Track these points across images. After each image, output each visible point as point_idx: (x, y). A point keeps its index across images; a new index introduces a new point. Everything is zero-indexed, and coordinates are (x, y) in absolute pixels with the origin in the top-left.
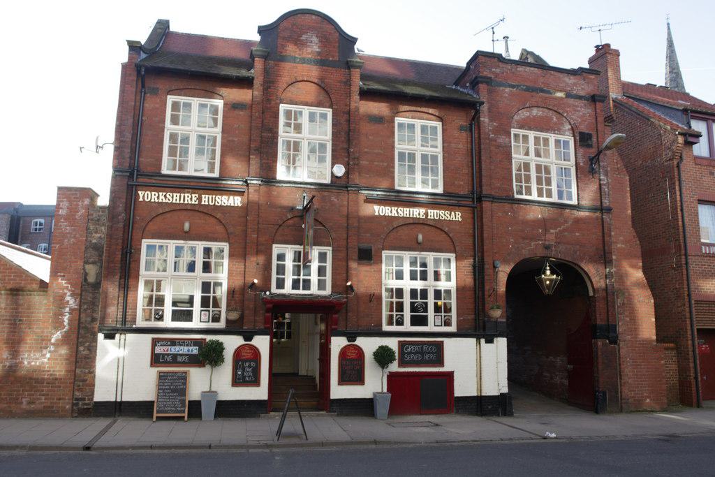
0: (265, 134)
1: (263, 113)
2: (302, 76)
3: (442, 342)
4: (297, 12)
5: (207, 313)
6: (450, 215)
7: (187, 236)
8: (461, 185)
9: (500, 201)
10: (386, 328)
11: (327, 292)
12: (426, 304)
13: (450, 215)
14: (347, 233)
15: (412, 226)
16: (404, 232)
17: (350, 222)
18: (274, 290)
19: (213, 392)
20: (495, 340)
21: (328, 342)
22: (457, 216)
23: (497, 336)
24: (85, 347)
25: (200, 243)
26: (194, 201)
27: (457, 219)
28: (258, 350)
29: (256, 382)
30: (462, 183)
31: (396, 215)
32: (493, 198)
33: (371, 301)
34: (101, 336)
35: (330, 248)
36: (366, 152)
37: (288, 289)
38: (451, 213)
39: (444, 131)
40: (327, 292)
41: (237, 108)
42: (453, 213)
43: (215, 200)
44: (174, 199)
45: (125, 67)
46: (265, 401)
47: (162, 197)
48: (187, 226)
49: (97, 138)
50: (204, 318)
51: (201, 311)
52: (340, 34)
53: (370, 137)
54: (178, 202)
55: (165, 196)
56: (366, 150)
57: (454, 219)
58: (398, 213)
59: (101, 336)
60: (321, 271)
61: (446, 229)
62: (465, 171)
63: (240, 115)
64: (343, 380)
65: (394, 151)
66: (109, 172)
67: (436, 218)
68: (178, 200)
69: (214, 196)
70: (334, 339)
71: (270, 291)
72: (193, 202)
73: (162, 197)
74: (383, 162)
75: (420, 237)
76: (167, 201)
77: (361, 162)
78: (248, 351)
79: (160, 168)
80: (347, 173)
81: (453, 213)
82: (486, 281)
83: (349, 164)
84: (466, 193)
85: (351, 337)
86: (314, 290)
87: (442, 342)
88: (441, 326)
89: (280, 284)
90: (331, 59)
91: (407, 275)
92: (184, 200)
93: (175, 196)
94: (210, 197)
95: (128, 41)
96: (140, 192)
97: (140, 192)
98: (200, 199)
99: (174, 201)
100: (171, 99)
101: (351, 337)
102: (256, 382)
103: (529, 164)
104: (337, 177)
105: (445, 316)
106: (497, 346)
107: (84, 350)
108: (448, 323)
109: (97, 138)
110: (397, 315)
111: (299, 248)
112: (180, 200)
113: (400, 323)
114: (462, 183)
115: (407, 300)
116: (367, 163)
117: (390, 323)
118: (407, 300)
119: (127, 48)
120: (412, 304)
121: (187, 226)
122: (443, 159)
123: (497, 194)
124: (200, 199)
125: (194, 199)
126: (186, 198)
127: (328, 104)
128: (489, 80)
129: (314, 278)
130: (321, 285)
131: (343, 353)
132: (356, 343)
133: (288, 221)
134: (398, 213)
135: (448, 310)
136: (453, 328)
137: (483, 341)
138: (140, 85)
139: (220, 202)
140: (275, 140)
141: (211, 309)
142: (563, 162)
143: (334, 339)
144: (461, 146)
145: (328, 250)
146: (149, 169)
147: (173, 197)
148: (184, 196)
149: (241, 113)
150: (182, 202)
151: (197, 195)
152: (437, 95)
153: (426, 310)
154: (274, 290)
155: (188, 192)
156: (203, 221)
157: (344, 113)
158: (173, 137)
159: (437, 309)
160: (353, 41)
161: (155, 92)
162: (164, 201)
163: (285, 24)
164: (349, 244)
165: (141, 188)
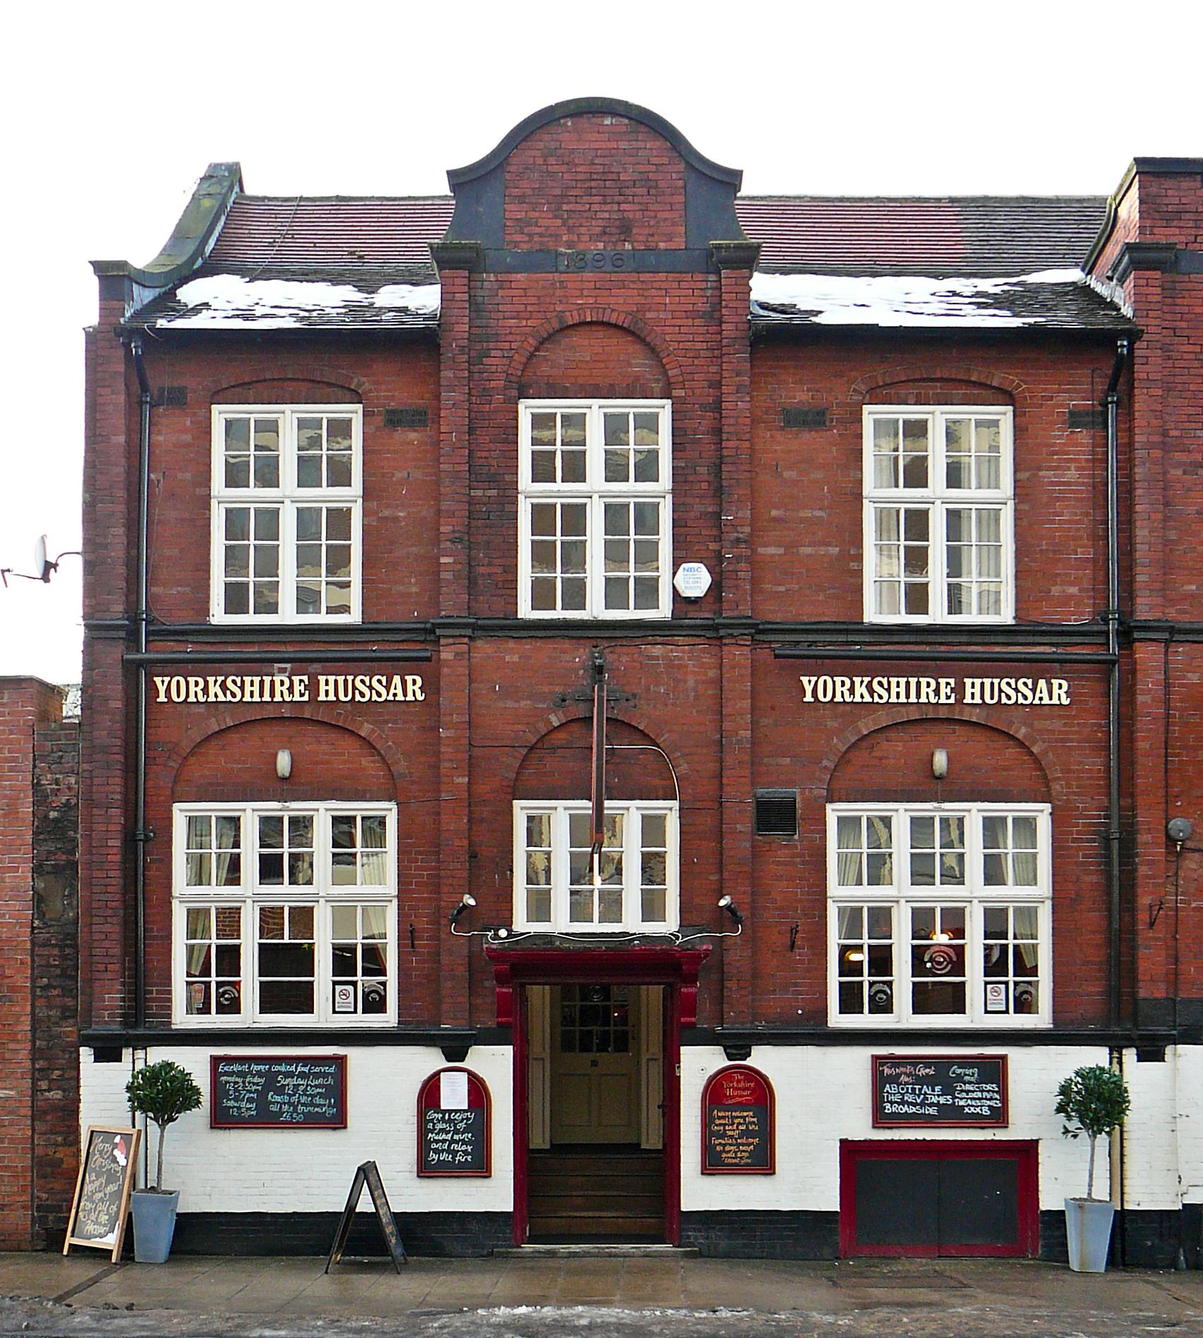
0: (480, 493)
1: (471, 431)
2: (581, 308)
3: (1004, 1058)
4: (621, 110)
5: (351, 988)
6: (1034, 690)
7: (288, 788)
8: (1072, 596)
9: (1190, 637)
10: (837, 1020)
11: (670, 924)
12: (960, 950)
13: (1034, 690)
14: (721, 761)
15: (919, 729)
16: (895, 749)
17: (726, 726)
18: (522, 923)
19: (165, 1192)
20: (1169, 1050)
21: (672, 1061)
22: (1058, 692)
23: (1175, 1042)
24: (51, 1081)
25: (901, 806)
26: (946, 696)
27: (1055, 701)
28: (764, 1078)
29: (480, 1167)
30: (1073, 590)
31: (868, 699)
32: (1172, 630)
33: (792, 947)
34: (86, 1054)
35: (675, 804)
36: (775, 519)
37: (561, 922)
38: (1035, 684)
39: (1019, 431)
40: (670, 924)
41: (399, 422)
42: (1042, 683)
43: (354, 688)
44: (247, 694)
45: (92, 338)
46: (510, 1212)
47: (860, 690)
48: (284, 762)
49: (43, 539)
50: (346, 1003)
51: (986, 983)
52: (690, 166)
53: (786, 474)
54: (257, 698)
55: (224, 687)
56: (774, 513)
57: (1046, 701)
58: (871, 692)
59: (86, 1054)
60: (652, 867)
61: (1021, 733)
62: (1084, 552)
63: (411, 443)
64: (713, 1164)
65: (515, 503)
66: (76, 635)
67: (988, 700)
68: (257, 694)
69: (350, 678)
70: (689, 1054)
71: (508, 924)
72: (297, 698)
73: (860, 690)
74: (829, 544)
75: (940, 760)
76: (229, 698)
77: (762, 550)
78: (742, 1085)
79: (206, 612)
80: (716, 588)
81: (1042, 683)
82: (1140, 881)
83: (719, 557)
84: (1086, 619)
85: (738, 1047)
86: (632, 922)
87: (1004, 1058)
88: (1007, 1012)
89: (540, 907)
90: (662, 245)
91: (975, 867)
92: (272, 694)
93: (893, 685)
94: (341, 679)
95: (90, 262)
96: (158, 680)
97: (158, 680)
98: (313, 687)
99: (247, 698)
100: (220, 414)
101: (738, 1047)
102: (480, 1167)
103: (925, 513)
104: (688, 600)
105: (219, 984)
106: (1175, 1069)
107: (49, 1090)
108: (375, 1004)
109: (43, 539)
110: (871, 984)
111: (584, 806)
112: (261, 695)
113: (883, 1005)
114: (1073, 590)
115: (249, 941)
116: (781, 551)
117: (850, 1002)
118: (249, 941)
119: (94, 283)
120: (918, 953)
121: (284, 762)
122: (1016, 519)
123: (1187, 618)
124: (313, 687)
125: (944, 690)
126: (924, 689)
127: (657, 387)
128: (1170, 255)
129: (632, 885)
130: (652, 908)
131: (714, 1092)
132: (748, 1062)
133: (554, 736)
134: (871, 692)
135: (1026, 968)
136: (1041, 1019)
137: (1130, 1055)
138: (136, 388)
139: (1021, 687)
140: (508, 508)
141: (1011, 978)
142: (903, 492)
143: (689, 1054)
144: (1072, 474)
145: (670, 811)
146: (181, 619)
147: (242, 688)
148: (272, 682)
149: (413, 436)
150: (267, 698)
151: (305, 678)
152: (1016, 322)
153: (959, 968)
154: (522, 923)
155: (282, 671)
156: (324, 747)
157: (704, 407)
158: (542, 515)
159: (994, 967)
160: (732, 179)
161: (177, 399)
162: (221, 698)
163: (529, 154)
164: (726, 789)
165: (159, 669)
